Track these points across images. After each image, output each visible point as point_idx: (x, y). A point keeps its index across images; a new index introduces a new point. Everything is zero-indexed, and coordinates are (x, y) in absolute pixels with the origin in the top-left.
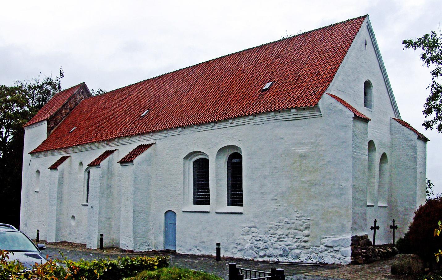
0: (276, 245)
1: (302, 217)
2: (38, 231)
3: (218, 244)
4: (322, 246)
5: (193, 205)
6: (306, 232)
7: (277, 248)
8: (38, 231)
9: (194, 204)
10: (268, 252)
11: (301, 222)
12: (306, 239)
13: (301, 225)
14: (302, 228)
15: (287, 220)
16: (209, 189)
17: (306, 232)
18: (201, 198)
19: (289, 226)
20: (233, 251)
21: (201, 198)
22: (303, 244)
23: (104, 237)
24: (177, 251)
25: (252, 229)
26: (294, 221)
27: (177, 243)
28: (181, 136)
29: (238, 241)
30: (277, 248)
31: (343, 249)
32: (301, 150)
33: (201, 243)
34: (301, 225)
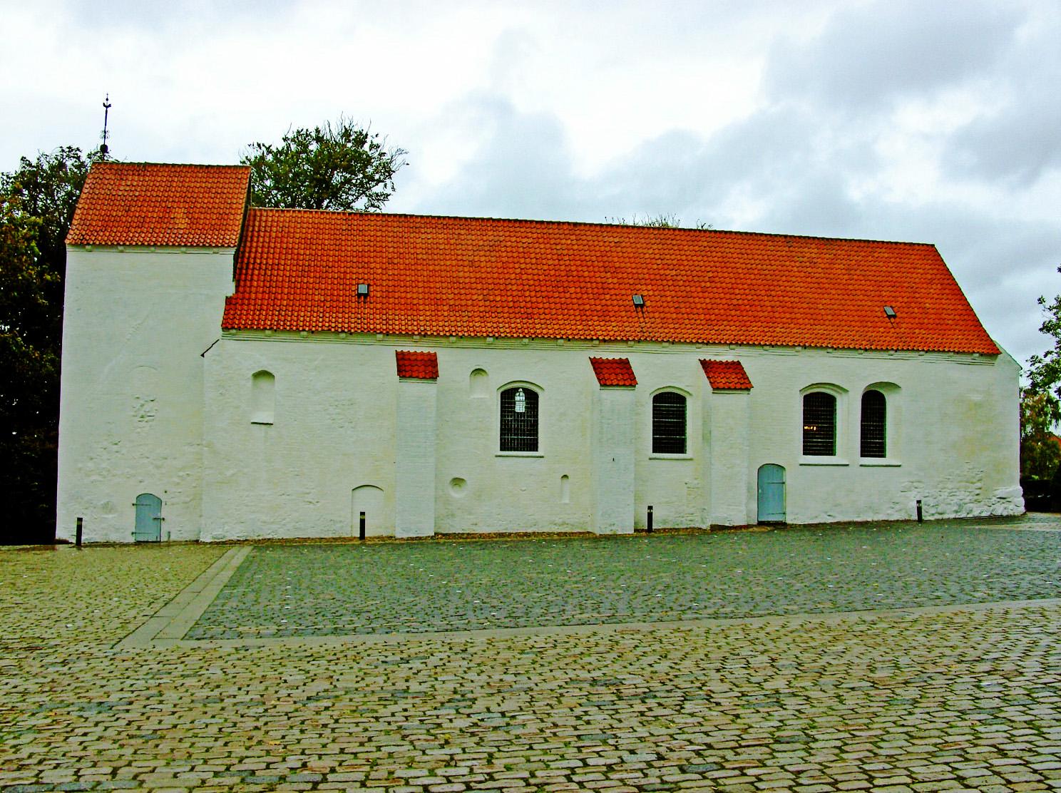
0: (948, 501)
1: (974, 468)
2: (80, 520)
3: (919, 502)
4: (994, 498)
5: (539, 449)
6: (979, 485)
7: (950, 504)
8: (80, 520)
9: (804, 454)
10: (940, 510)
11: (974, 475)
12: (978, 492)
13: (974, 477)
14: (974, 480)
15: (958, 472)
16: (654, 426)
17: (979, 485)
18: (820, 446)
19: (959, 479)
20: (889, 512)
21: (820, 446)
22: (976, 497)
23: (367, 518)
24: (789, 522)
25: (915, 484)
26: (965, 473)
27: (788, 511)
28: (796, 358)
29: (896, 500)
30: (950, 504)
31: (1016, 500)
32: (977, 398)
33: (836, 506)
34: (974, 477)
